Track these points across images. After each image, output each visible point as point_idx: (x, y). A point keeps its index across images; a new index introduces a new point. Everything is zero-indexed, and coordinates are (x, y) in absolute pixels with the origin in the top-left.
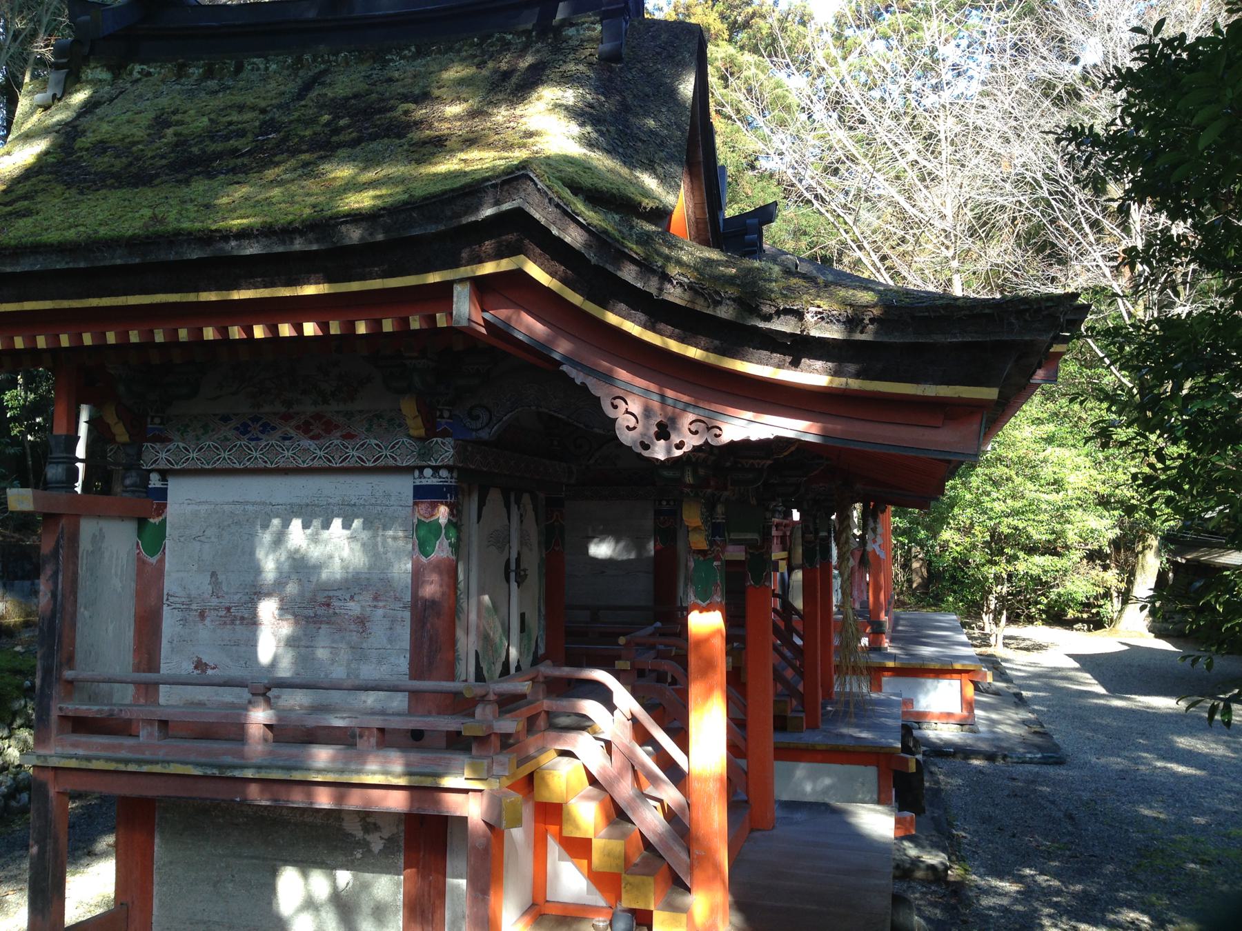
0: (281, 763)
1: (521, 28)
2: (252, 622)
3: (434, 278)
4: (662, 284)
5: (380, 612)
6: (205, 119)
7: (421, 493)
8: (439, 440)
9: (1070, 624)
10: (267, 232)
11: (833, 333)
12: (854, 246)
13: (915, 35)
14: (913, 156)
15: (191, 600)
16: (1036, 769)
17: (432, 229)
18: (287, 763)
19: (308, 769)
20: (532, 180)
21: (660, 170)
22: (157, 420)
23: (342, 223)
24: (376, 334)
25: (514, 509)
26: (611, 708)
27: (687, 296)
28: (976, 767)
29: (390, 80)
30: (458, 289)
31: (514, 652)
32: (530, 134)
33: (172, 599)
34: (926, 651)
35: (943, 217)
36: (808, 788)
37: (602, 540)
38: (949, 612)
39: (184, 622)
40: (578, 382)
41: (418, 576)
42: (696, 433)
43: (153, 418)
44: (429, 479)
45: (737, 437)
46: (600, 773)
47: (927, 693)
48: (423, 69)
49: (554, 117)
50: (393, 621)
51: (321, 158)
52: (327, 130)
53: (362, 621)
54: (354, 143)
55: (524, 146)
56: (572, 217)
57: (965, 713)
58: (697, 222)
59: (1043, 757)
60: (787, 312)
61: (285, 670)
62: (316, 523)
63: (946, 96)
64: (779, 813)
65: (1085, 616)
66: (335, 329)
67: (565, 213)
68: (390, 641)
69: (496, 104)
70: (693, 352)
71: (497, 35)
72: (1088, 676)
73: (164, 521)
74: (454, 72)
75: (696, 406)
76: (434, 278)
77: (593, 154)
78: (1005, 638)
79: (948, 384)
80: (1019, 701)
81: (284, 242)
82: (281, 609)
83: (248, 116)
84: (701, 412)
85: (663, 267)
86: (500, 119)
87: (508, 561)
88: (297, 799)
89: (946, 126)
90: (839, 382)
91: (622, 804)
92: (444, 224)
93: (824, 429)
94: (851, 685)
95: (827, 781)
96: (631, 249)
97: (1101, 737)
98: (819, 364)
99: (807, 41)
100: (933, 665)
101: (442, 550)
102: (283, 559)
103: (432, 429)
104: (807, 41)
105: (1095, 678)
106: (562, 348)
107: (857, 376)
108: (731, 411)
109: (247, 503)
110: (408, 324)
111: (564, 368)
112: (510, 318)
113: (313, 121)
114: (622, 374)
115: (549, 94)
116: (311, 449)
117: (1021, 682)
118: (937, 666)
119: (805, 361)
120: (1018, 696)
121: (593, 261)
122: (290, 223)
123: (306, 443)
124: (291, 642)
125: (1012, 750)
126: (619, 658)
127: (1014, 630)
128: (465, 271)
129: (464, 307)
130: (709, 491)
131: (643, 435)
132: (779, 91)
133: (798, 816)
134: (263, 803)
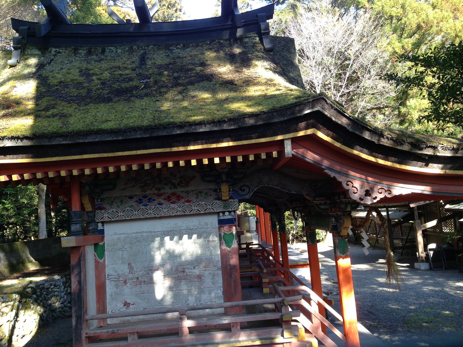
2: (151, 282)
3: (280, 138)
5: (207, 273)
7: (222, 223)
8: (232, 200)
11: (448, 154)
15: (119, 276)
17: (282, 119)
22: (99, 200)
30: (286, 142)
33: (110, 277)
39: (117, 286)
40: (332, 176)
43: (97, 199)
50: (214, 275)
53: (200, 277)
60: (430, 147)
62: (176, 238)
68: (213, 283)
70: (389, 164)
71: (217, 41)
72: (330, 259)
73: (104, 243)
76: (280, 138)
93: (432, 189)
94: (326, 275)
98: (435, 165)
106: (326, 163)
109: (143, 232)
111: (326, 171)
114: (352, 173)
116: (177, 207)
118: (302, 263)
119: (430, 165)
121: (350, 130)
124: (170, 288)
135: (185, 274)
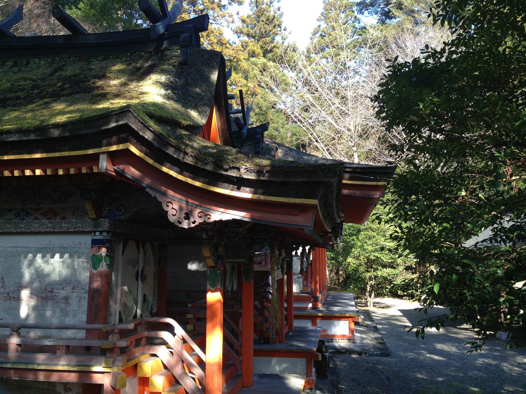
0: (23, 361)
1: (148, 50)
2: (18, 299)
3: (90, 152)
4: (184, 156)
5: (75, 294)
6: (9, 84)
7: (95, 243)
8: (103, 220)
9: (401, 297)
10: (19, 131)
11: (252, 176)
12: (314, 141)
13: (338, 57)
14: (337, 105)
16: (377, 358)
17: (90, 131)
18: (27, 361)
19: (34, 364)
20: (131, 112)
21: (200, 109)
23: (51, 128)
24: (67, 175)
25: (141, 248)
26: (174, 335)
27: (194, 161)
28: (353, 358)
29: (91, 69)
30: (101, 156)
31: (139, 311)
32: (142, 93)
34: (336, 309)
35: (349, 130)
36: (278, 368)
37: (193, 263)
38: (350, 292)
40: (153, 196)
41: (91, 277)
42: (200, 217)
44: (98, 236)
45: (217, 219)
46: (167, 363)
47: (336, 326)
48: (105, 65)
49: (155, 87)
50: (81, 299)
51: (53, 100)
52: (59, 89)
54: (68, 95)
55: (138, 98)
56: (148, 128)
57: (351, 335)
58: (222, 130)
59: (381, 353)
60: (234, 168)
61: (31, 321)
62: (48, 256)
63: (351, 81)
64: (255, 379)
65: (405, 293)
66: (49, 172)
67: (145, 126)
68: (79, 307)
69: (132, 81)
70: (198, 184)
71: (137, 53)
72: (405, 319)
74: (118, 67)
75: (201, 206)
76: (90, 152)
77: (168, 102)
78: (374, 303)
79: (299, 198)
80: (376, 330)
81: (25, 136)
82: (31, 293)
83: (28, 82)
84: (203, 209)
85: (185, 149)
86: (132, 86)
87: (138, 271)
88: (30, 377)
89: (349, 94)
90: (256, 197)
91: (177, 377)
92: (93, 131)
93: (252, 216)
95: (285, 365)
96: (172, 141)
97: (406, 344)
98: (248, 189)
99: (295, 58)
100: (337, 315)
101: (103, 267)
102: (33, 271)
103: (99, 215)
104: (295, 58)
105: (408, 320)
106: (147, 181)
107: (263, 194)
108: (214, 208)
109: (18, 247)
110: (57, 172)
111: (147, 190)
112: (124, 169)
113: (55, 85)
114: (171, 192)
115: (154, 77)
116: (46, 224)
117: (378, 321)
120: (375, 327)
121: (156, 146)
122: (28, 128)
123: (44, 221)
124: (35, 308)
125: (369, 350)
126: (189, 313)
127: (378, 300)
128: (104, 149)
129: (104, 164)
130: (214, 241)
131: (179, 218)
132: (284, 78)
133: (265, 380)
134: (16, 379)
135: (53, 294)
